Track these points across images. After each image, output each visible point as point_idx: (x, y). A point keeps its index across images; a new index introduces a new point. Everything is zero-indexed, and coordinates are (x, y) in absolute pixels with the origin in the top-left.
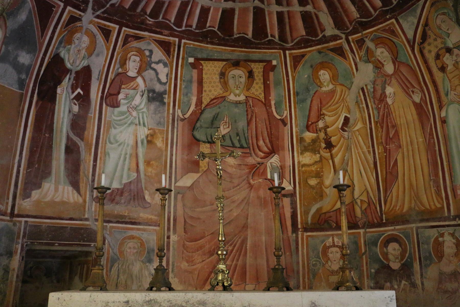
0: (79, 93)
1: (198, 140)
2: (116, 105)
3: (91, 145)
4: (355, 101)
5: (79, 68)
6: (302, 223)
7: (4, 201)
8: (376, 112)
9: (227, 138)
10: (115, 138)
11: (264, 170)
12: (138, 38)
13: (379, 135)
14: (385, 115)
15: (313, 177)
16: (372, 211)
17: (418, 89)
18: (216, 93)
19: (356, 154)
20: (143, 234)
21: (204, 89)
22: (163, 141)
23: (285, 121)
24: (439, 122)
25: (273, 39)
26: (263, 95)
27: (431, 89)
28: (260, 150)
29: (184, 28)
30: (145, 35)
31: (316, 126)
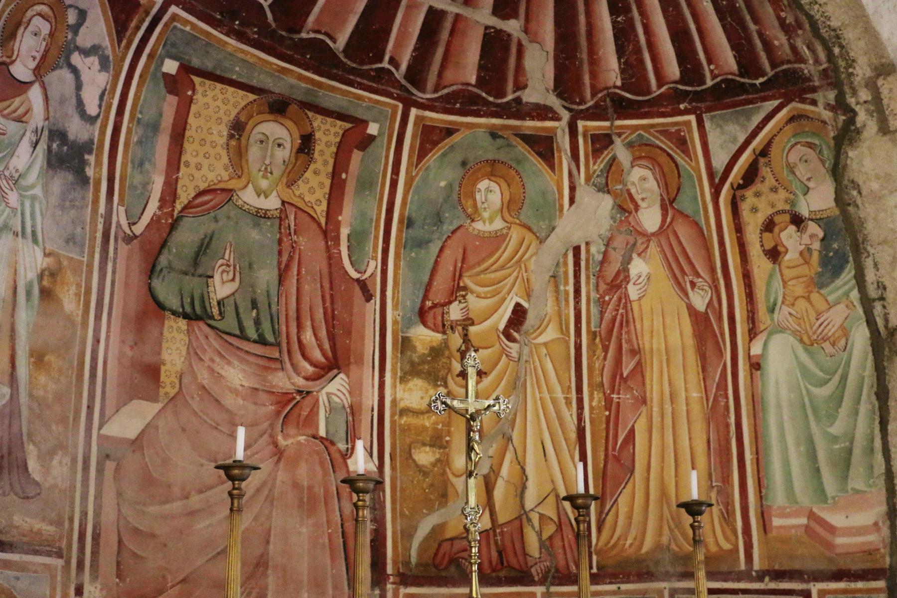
1: (161, 306)
4: (551, 274)
6: (395, 563)
8: (594, 310)
9: (230, 310)
11: (312, 410)
13: (597, 365)
14: (618, 321)
15: (424, 444)
16: (566, 543)
17: (706, 282)
18: (211, 176)
19: (535, 403)
20: (18, 579)
21: (183, 159)
22: (78, 295)
23: (370, 288)
24: (744, 365)
25: (393, 69)
26: (324, 206)
28: (305, 357)
31: (443, 313)
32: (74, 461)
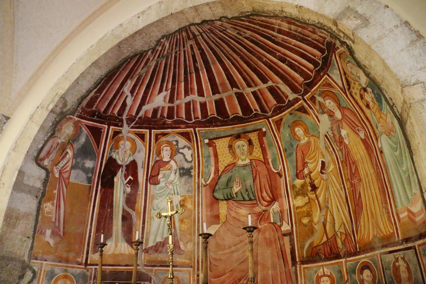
0: (130, 179)
1: (217, 199)
2: (157, 183)
3: (141, 213)
5: (128, 163)
6: (299, 257)
7: (81, 255)
8: (340, 153)
9: (239, 194)
10: (157, 206)
11: (268, 215)
12: (164, 135)
14: (347, 154)
15: (305, 217)
19: (333, 192)
20: (179, 274)
21: (219, 161)
22: (192, 203)
27: (368, 125)
28: (264, 200)
29: (194, 121)
30: (169, 131)
32: (194, 244)
